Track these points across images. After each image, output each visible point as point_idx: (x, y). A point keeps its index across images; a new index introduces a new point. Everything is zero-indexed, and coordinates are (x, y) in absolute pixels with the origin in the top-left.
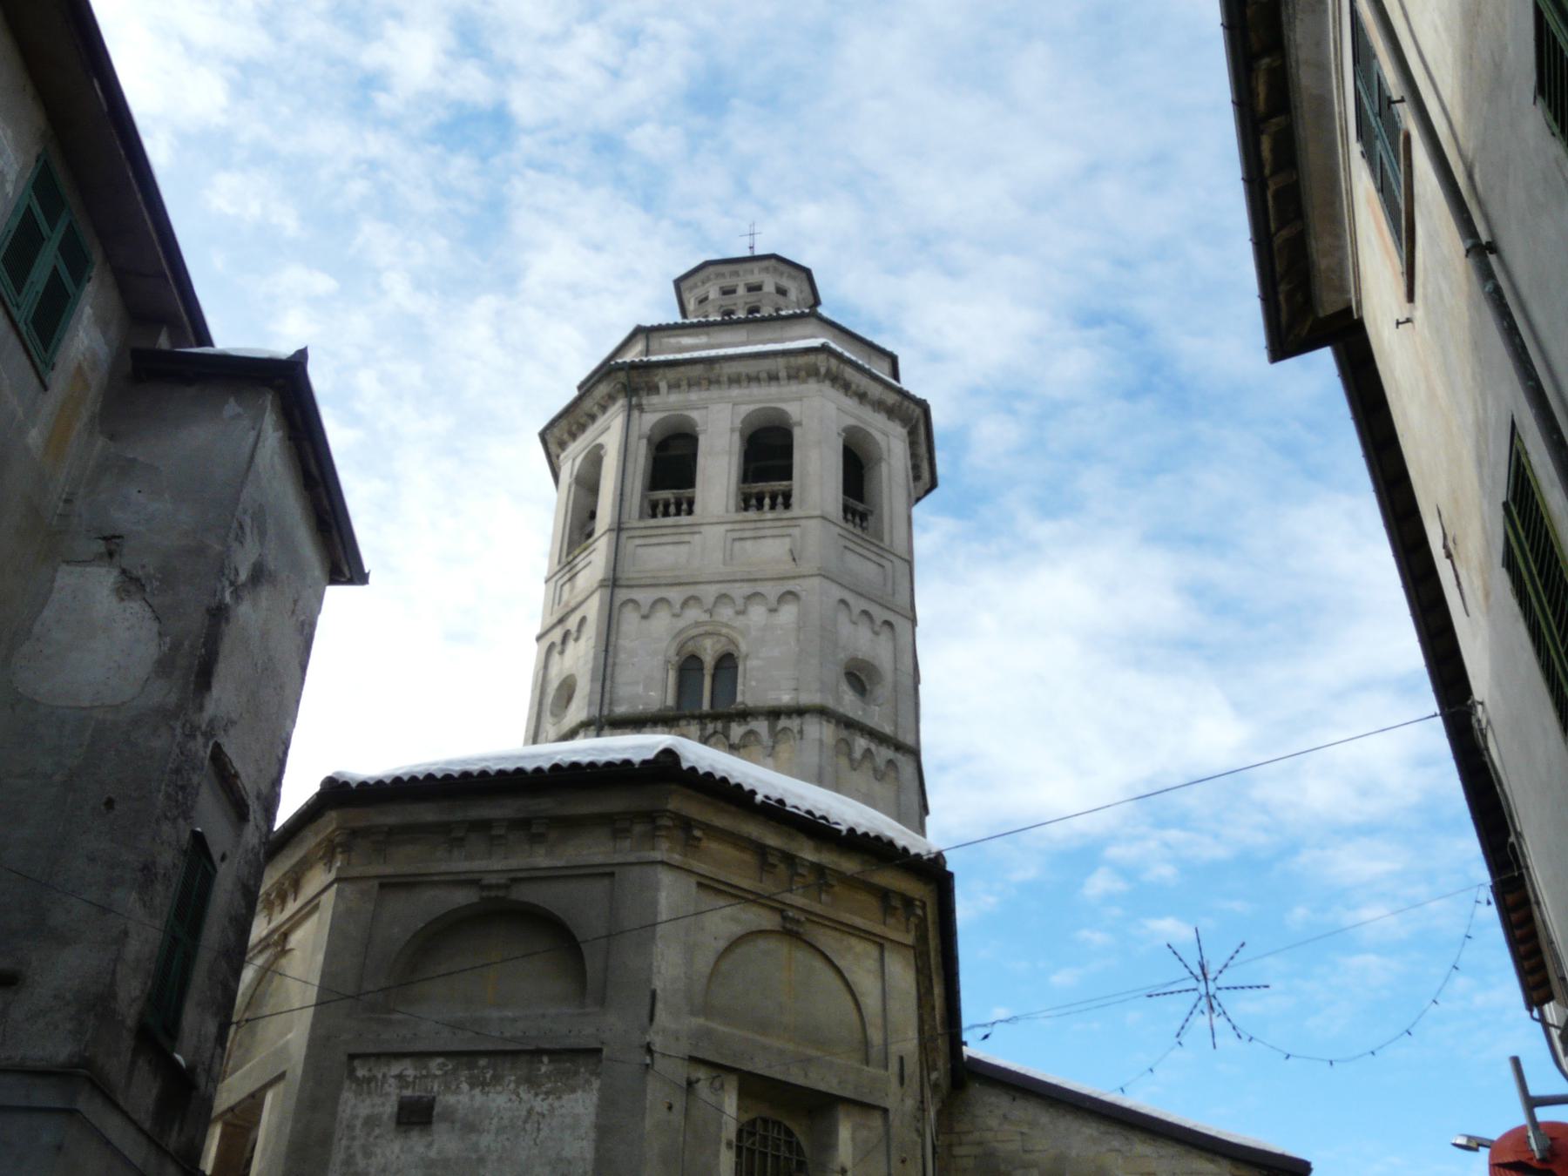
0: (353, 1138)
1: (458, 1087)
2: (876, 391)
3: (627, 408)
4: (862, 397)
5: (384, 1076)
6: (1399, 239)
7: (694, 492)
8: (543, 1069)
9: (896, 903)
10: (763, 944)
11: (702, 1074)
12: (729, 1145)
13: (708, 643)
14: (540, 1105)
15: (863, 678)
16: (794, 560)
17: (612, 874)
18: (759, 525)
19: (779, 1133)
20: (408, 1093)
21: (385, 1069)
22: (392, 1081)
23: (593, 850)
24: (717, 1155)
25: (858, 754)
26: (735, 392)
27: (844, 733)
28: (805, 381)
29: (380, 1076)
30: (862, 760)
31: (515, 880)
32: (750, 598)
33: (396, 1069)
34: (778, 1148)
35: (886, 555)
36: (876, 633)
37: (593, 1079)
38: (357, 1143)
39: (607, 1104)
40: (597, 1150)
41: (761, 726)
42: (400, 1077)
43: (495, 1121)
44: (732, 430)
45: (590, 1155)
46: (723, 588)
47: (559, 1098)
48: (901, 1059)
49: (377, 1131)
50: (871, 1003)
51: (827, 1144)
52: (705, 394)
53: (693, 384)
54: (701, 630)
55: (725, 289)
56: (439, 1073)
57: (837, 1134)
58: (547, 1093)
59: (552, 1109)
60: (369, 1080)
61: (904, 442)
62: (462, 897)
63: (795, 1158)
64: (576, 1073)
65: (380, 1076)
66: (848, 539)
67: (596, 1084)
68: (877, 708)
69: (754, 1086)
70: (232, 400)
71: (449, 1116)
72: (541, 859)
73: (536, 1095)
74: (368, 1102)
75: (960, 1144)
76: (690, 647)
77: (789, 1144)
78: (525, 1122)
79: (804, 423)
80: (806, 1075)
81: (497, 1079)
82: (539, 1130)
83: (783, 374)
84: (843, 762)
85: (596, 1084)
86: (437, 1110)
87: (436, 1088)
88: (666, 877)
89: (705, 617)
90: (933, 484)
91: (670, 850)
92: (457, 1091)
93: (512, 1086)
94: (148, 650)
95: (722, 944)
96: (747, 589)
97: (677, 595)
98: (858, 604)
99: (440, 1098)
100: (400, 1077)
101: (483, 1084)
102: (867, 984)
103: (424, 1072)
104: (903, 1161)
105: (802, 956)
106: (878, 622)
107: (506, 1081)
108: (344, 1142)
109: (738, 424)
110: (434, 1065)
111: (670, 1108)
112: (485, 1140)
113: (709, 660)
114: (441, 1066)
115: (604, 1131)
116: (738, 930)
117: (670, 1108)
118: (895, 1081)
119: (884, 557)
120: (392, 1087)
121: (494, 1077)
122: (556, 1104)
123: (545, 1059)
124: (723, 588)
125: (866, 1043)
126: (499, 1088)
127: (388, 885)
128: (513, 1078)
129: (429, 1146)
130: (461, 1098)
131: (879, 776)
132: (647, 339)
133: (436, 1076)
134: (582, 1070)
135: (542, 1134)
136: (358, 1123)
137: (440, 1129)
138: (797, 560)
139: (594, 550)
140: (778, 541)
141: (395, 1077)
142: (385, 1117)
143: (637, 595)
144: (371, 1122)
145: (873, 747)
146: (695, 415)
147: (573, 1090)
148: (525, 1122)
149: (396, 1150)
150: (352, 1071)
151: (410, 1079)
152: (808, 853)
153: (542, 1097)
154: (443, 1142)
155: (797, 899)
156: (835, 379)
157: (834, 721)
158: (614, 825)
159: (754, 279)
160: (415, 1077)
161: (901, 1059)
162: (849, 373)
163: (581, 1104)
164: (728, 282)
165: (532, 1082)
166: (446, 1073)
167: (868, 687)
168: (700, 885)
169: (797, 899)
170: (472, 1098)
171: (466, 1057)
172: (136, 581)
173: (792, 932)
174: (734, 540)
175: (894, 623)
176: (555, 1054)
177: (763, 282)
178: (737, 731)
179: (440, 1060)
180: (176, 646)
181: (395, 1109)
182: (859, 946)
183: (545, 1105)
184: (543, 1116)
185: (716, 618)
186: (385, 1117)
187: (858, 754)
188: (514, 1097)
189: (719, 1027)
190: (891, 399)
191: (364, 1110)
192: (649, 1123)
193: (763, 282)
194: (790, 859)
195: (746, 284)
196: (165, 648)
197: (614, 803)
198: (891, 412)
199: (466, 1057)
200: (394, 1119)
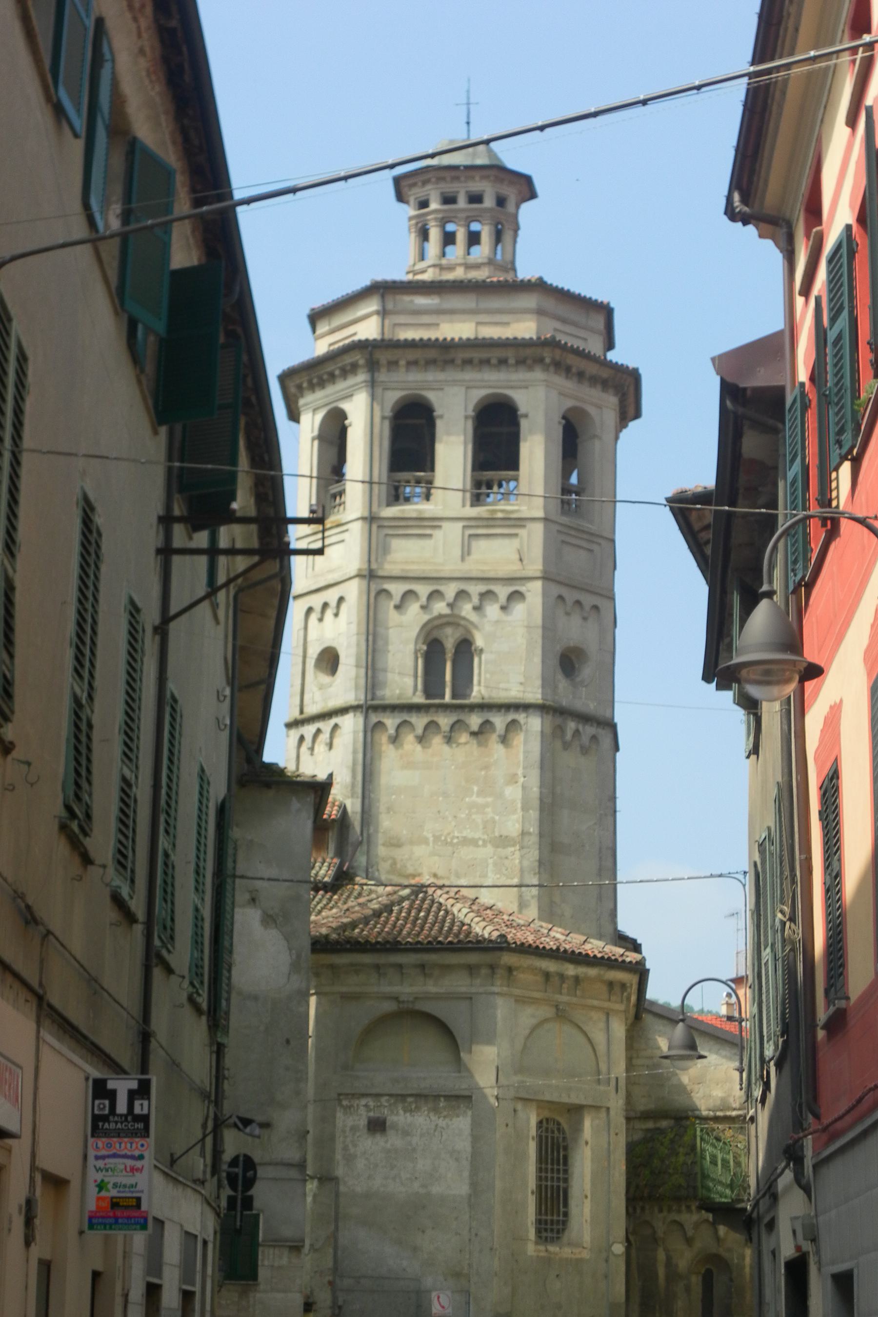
0: (346, 1137)
1: (397, 1112)
2: (592, 369)
3: (369, 384)
4: (581, 375)
5: (358, 1105)
6: (766, 1183)
7: (433, 476)
8: (441, 1105)
9: (617, 989)
10: (547, 1026)
11: (519, 1106)
12: (533, 1138)
13: (449, 631)
14: (442, 1122)
15: (573, 658)
16: (521, 560)
17: (471, 998)
18: (491, 523)
19: (554, 1124)
20: (371, 1114)
21: (357, 1102)
22: (362, 1108)
23: (459, 983)
24: (528, 1144)
25: (569, 736)
26: (469, 375)
27: (559, 720)
28: (530, 368)
29: (355, 1105)
30: (572, 740)
31: (416, 998)
32: (484, 596)
33: (363, 1102)
34: (553, 1132)
35: (596, 540)
36: (585, 619)
37: (468, 1110)
38: (348, 1140)
39: (476, 1124)
40: (473, 1147)
41: (499, 721)
42: (366, 1106)
43: (419, 1131)
44: (466, 417)
45: (469, 1149)
46: (463, 586)
47: (451, 1120)
48: (617, 1079)
49: (358, 1134)
50: (601, 1048)
51: (578, 1128)
52: (441, 376)
53: (430, 363)
54: (444, 620)
55: (446, 195)
56: (386, 1104)
57: (583, 1125)
58: (445, 1117)
59: (448, 1126)
60: (350, 1107)
61: (615, 410)
62: (389, 1007)
63: (561, 1136)
64: (459, 1107)
65: (355, 1105)
66: (565, 533)
67: (469, 1113)
68: (584, 689)
69: (541, 1104)
70: (294, 798)
71: (395, 1127)
72: (432, 988)
73: (439, 1118)
74: (351, 1118)
75: (638, 1057)
76: (431, 637)
77: (559, 1130)
78: (435, 1131)
79: (530, 415)
80: (569, 1097)
81: (418, 1109)
82: (442, 1136)
83: (512, 361)
84: (558, 744)
85: (469, 1113)
86: (388, 1124)
87: (386, 1112)
88: (500, 1001)
89: (446, 611)
90: (637, 415)
91: (501, 986)
92: (397, 1114)
93: (426, 1112)
94: (284, 959)
95: (527, 1032)
96: (482, 588)
97: (423, 590)
98: (571, 596)
99: (388, 1118)
100: (366, 1106)
101: (411, 1111)
102: (599, 1037)
103: (379, 1104)
104: (617, 1134)
105: (567, 1028)
106: (587, 608)
107: (423, 1110)
108: (341, 1139)
109: (471, 413)
110: (384, 1100)
111: (507, 1125)
112: (415, 1140)
113: (450, 645)
114: (388, 1101)
115: (475, 1139)
116: (534, 1021)
117: (507, 1125)
118: (614, 1091)
119: (593, 542)
120: (362, 1111)
121: (416, 1107)
122: (450, 1123)
123: (442, 1099)
124: (463, 586)
125: (599, 1072)
126: (419, 1114)
127: (347, 997)
128: (426, 1108)
129: (386, 1142)
130: (399, 1118)
131: (585, 751)
132: (383, 297)
133: (386, 1107)
134: (462, 1106)
135: (444, 1137)
136: (348, 1129)
137: (391, 1133)
138: (525, 562)
139: (347, 530)
140: (506, 542)
141: (364, 1106)
142: (361, 1127)
143: (391, 587)
144: (354, 1129)
145: (581, 728)
146: (432, 396)
147: (458, 1116)
148: (435, 1131)
149: (369, 1144)
150: (340, 1101)
151: (372, 1107)
152: (571, 970)
153: (442, 1119)
154: (393, 1140)
155: (564, 998)
156: (558, 366)
157: (551, 713)
158: (471, 970)
159: (476, 186)
160: (374, 1106)
161: (617, 1079)
162: (571, 360)
163: (462, 1123)
164: (449, 187)
165: (436, 1110)
166: (390, 1105)
167: (577, 666)
168: (516, 1001)
169: (564, 998)
170: (406, 1118)
171: (402, 1097)
172: (270, 916)
173: (561, 1014)
174: (470, 536)
175: (600, 607)
176: (447, 1097)
177: (484, 191)
178: (475, 721)
179: (387, 1098)
180: (299, 956)
181: (366, 1123)
182: (595, 1015)
183: (444, 1122)
184: (443, 1128)
185: (456, 611)
186: (361, 1127)
187: (569, 736)
188: (428, 1119)
189: (529, 1081)
190: (605, 373)
191: (350, 1122)
192: (498, 1135)
193: (484, 191)
194: (562, 977)
195: (467, 192)
196: (294, 957)
197: (473, 958)
198: (605, 384)
199: (402, 1097)
200: (366, 1128)
